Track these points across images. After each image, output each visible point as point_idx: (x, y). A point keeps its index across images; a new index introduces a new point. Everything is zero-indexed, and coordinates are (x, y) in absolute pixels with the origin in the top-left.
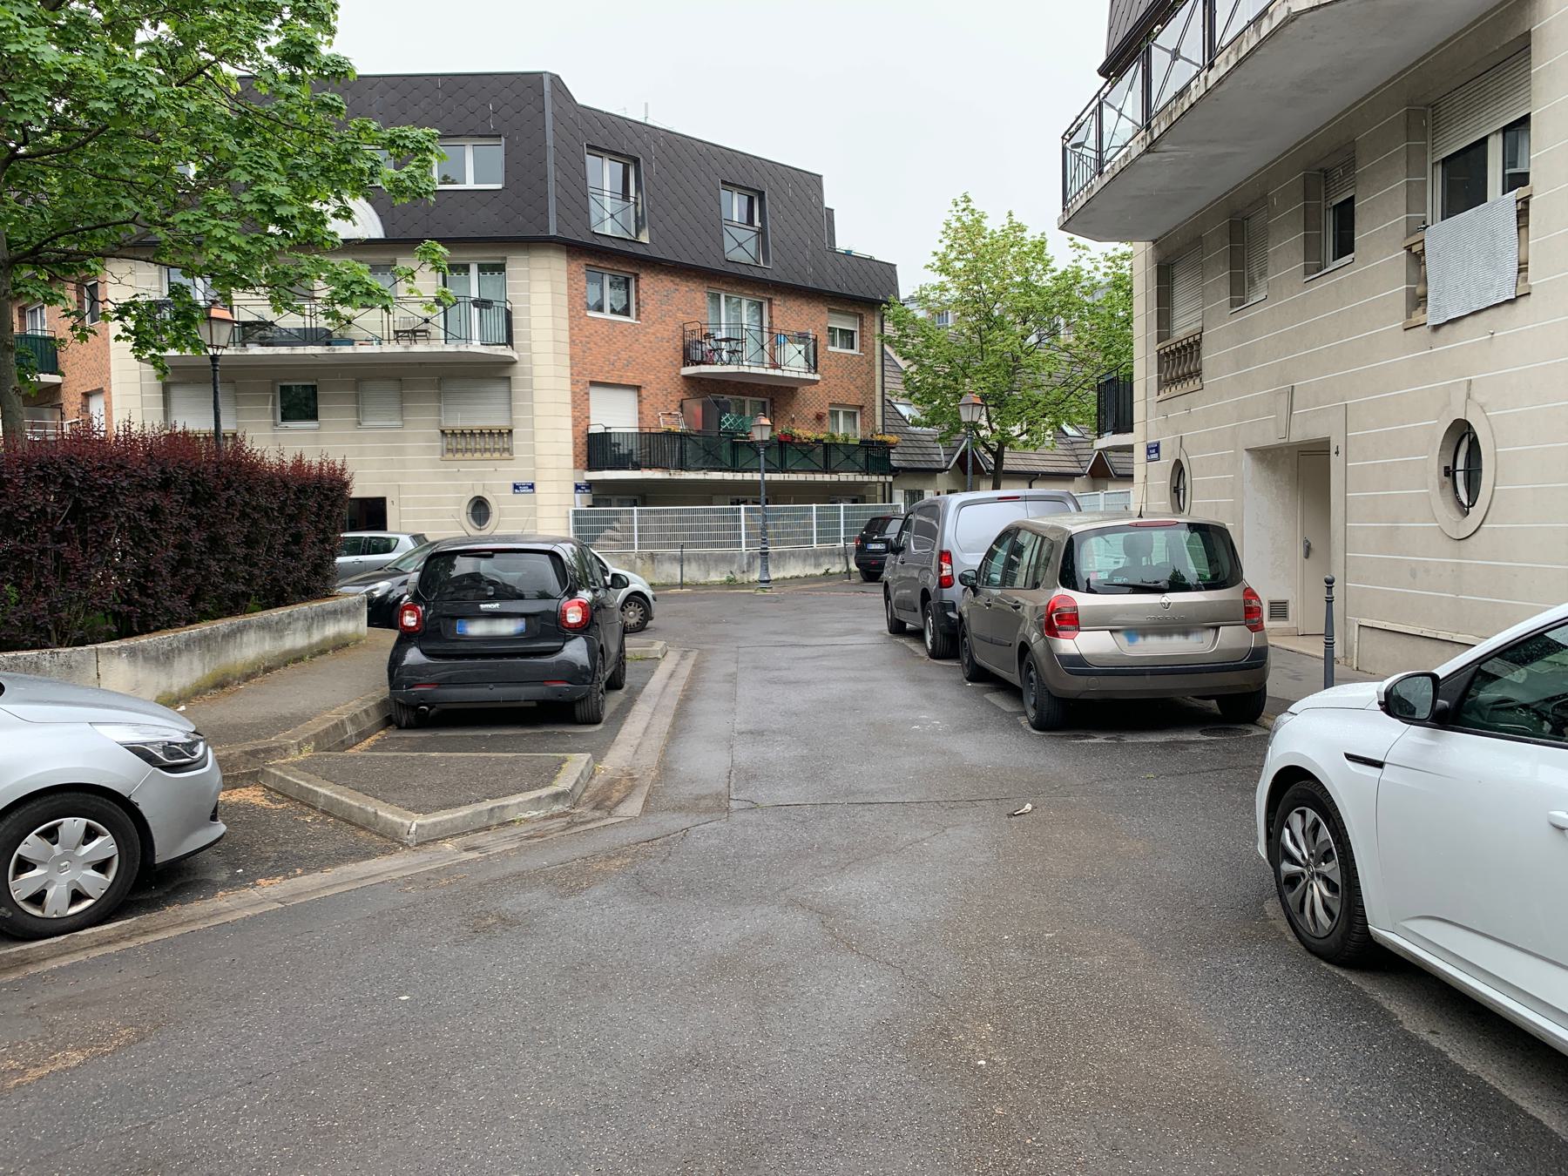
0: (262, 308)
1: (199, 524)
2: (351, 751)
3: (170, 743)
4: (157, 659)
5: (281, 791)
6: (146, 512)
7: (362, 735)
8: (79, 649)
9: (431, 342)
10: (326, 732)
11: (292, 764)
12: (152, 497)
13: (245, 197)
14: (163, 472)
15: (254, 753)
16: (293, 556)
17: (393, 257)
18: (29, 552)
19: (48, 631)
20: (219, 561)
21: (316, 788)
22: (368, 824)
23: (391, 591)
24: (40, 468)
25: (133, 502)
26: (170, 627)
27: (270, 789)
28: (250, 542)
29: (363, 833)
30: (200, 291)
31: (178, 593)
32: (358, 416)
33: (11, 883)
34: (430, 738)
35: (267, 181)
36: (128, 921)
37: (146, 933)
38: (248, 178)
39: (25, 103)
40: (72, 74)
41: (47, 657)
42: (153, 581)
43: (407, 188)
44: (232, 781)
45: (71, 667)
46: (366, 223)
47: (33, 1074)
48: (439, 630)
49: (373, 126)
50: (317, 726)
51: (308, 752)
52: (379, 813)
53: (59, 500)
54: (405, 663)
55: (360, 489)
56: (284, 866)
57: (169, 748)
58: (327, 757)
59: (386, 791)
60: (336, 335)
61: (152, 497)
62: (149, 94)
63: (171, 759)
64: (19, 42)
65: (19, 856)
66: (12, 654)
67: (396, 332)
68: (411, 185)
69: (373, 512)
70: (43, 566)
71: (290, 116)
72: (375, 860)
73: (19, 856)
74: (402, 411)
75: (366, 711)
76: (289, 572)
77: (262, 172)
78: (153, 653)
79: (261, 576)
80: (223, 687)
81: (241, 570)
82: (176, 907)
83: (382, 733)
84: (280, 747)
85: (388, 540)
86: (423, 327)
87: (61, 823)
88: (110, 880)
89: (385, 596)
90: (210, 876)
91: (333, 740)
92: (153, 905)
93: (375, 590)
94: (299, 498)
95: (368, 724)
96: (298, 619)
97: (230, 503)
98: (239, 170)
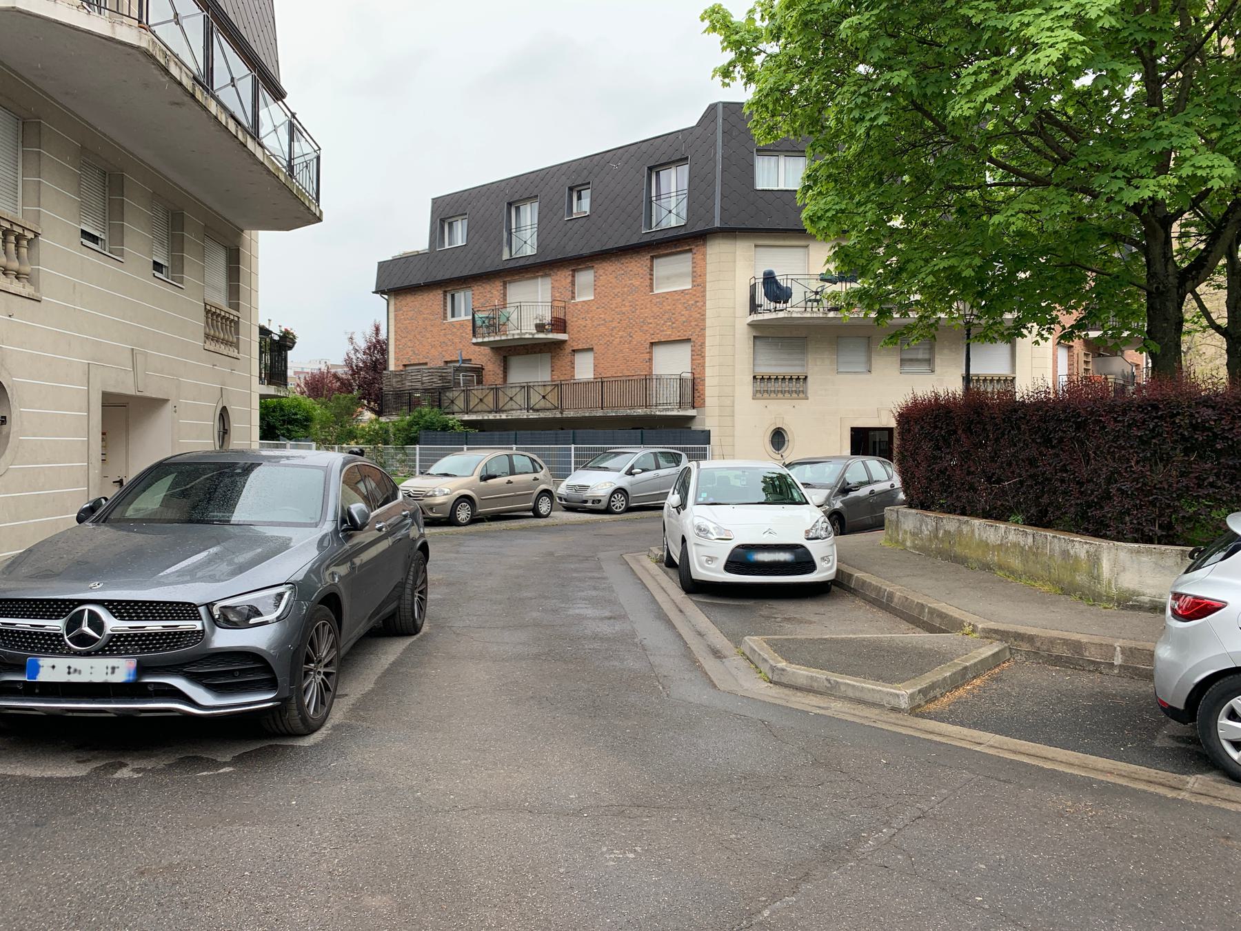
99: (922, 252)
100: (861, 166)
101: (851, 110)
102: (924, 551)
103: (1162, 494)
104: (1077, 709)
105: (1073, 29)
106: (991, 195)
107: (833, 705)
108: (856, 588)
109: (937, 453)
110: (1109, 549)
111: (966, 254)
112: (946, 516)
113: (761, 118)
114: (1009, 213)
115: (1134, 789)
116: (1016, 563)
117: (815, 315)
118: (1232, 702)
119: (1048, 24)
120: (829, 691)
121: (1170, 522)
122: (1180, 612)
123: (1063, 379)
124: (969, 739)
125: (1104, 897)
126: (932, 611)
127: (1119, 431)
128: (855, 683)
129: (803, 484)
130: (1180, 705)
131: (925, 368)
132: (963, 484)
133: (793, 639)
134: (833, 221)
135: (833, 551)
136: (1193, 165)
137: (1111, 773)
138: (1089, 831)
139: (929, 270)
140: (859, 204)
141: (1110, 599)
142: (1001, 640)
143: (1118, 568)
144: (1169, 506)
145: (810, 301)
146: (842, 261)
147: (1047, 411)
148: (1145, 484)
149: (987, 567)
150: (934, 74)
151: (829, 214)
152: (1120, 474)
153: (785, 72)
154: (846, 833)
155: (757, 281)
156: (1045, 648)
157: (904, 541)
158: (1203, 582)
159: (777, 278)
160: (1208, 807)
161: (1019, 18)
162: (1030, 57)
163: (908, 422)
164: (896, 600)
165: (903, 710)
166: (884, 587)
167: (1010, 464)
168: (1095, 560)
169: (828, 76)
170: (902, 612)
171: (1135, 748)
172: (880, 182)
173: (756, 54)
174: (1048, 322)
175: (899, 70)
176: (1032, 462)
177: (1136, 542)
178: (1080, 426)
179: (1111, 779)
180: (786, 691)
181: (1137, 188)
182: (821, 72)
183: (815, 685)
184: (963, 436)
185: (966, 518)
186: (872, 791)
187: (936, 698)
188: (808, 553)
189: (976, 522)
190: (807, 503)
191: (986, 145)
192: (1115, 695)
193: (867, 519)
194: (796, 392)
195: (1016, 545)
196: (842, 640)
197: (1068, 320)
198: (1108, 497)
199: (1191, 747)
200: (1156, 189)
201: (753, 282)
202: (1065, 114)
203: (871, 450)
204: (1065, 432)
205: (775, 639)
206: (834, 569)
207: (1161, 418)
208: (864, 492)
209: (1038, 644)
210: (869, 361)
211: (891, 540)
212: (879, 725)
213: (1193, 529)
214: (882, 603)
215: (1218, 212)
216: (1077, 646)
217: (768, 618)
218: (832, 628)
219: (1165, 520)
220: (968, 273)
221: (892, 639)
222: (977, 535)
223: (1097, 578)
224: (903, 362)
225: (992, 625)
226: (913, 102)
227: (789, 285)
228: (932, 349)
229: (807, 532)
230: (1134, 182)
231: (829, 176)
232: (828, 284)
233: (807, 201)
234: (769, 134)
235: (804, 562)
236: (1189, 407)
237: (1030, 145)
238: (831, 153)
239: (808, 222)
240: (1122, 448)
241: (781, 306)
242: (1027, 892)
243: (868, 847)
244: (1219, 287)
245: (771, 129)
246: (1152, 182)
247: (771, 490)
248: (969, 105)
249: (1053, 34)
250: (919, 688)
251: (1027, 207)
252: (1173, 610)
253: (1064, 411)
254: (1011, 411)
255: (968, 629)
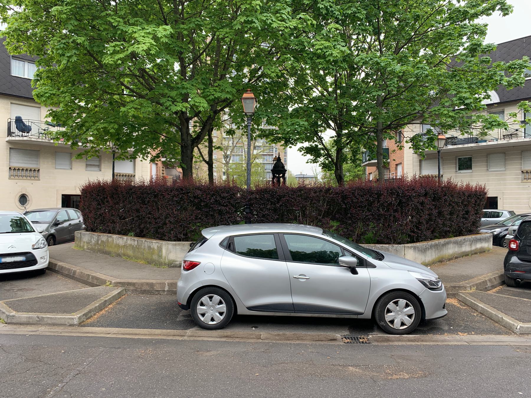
0: (453, 132)
1: (435, 207)
2: (488, 292)
3: (431, 281)
4: (422, 251)
5: (464, 302)
6: (420, 203)
7: (493, 287)
8: (399, 245)
9: (518, 138)
10: (480, 283)
11: (468, 293)
12: (422, 199)
13: (455, 99)
14: (425, 191)
15: (455, 287)
16: (466, 219)
17: (503, 108)
18: (387, 215)
19: (391, 239)
20: (441, 220)
21: (478, 304)
22: (499, 321)
23: (501, 233)
24: (391, 190)
25: (416, 200)
26: (425, 240)
27: (460, 301)
28: (451, 214)
29: (497, 324)
30: (435, 131)
31: (428, 229)
32: (487, 167)
33: (385, 315)
34: (522, 292)
35: (462, 92)
36: (417, 336)
37: (422, 341)
38: (455, 92)
39: (391, 84)
40: (404, 72)
41: (391, 247)
42: (421, 225)
43: (513, 83)
44: (449, 296)
45: (397, 251)
46: (495, 98)
47: (395, 377)
48: (526, 251)
49: (502, 63)
50: (476, 281)
51: (473, 290)
52: (504, 318)
53: (395, 200)
54: (511, 262)
55: (490, 194)
56: (467, 330)
57: (431, 282)
58: (481, 293)
59: (506, 310)
60: (480, 139)
61: (422, 199)
62: (426, 72)
63: (431, 286)
64: (391, 67)
65: (388, 308)
66: (381, 245)
67: (504, 136)
68: (514, 82)
69: (493, 202)
70: (390, 219)
71: (470, 68)
72: (503, 336)
73: (388, 308)
74: (505, 165)
75: (495, 278)
76: (464, 224)
77: (460, 90)
78: (420, 249)
79: (454, 225)
80: (441, 262)
81: (448, 223)
82: (432, 335)
83: (501, 287)
84: (464, 287)
85: (499, 213)
86: (515, 133)
87: (399, 300)
88: (412, 321)
89: (499, 234)
90: (442, 327)
91: (482, 287)
92: (424, 332)
93: (494, 232)
94: (468, 198)
95: (496, 283)
96: (467, 241)
97: (446, 201)
98: (453, 91)
99: (92, 119)
100: (64, 76)
101: (58, 49)
102: (93, 250)
103: (184, 223)
104: (150, 311)
105: (152, 39)
106: (124, 98)
107: (40, 329)
108: (59, 270)
109: (99, 207)
110: (165, 244)
111: (111, 122)
112: (102, 234)
113: (11, 41)
114: (128, 107)
115: (168, 340)
116: (130, 252)
117: (44, 141)
118: (201, 299)
119: (143, 34)
120: (39, 322)
121: (187, 233)
122: (186, 267)
123: (154, 177)
124: (105, 332)
125: (152, 388)
126: (93, 277)
127: (169, 198)
128: (52, 316)
129: (32, 222)
130: (185, 303)
131: (97, 169)
132: (110, 220)
133: (21, 300)
134: (49, 98)
135: (47, 254)
136: (194, 101)
137: (160, 335)
138: (149, 361)
139: (95, 127)
140: (63, 92)
141: (165, 264)
142: (122, 286)
143: (169, 252)
144: (186, 227)
145: (41, 133)
146: (54, 117)
147: (143, 190)
148: (178, 219)
149: (119, 255)
150: (98, 42)
151: (47, 95)
152: (169, 215)
153: (24, 22)
154: (39, 392)
155: (12, 120)
156: (139, 287)
157: (84, 246)
158: (193, 256)
159: (23, 120)
160: (194, 340)
161: (132, 29)
162: (136, 46)
163: (86, 193)
164: (77, 274)
165: (75, 325)
166: (72, 268)
167: (129, 212)
168: (160, 249)
169: (46, 30)
170: (80, 279)
171: (170, 323)
172: (73, 84)
173: (8, 9)
174: (145, 154)
175: (81, 36)
176: (138, 211)
177: (175, 241)
178: (155, 196)
179: (160, 337)
180: (15, 326)
181: (176, 106)
182: (42, 27)
183: (31, 320)
184: (110, 199)
185: (110, 235)
186: (55, 367)
187: (91, 316)
188: (33, 256)
189: (115, 236)
190: (34, 231)
191: (119, 78)
192: (165, 303)
193: (67, 237)
194: (21, 176)
195: (130, 245)
196: (48, 296)
197: (154, 153)
198: (165, 224)
199: (189, 318)
200: (182, 107)
201: (9, 120)
202: (154, 72)
203: (72, 205)
204: (150, 198)
205: (10, 301)
206: (48, 262)
207: (184, 194)
208: (66, 224)
209: (137, 286)
210: (71, 164)
211: (77, 246)
212: (63, 334)
213: (194, 235)
214: (71, 276)
215: (205, 119)
216: (152, 285)
217: (9, 290)
218: (44, 291)
219: (185, 232)
220: (112, 131)
221: (73, 292)
222: (115, 242)
223: (160, 256)
224: (87, 165)
225: (118, 280)
226: (88, 51)
227: (30, 125)
228: (100, 161)
229: (33, 245)
230: (175, 103)
231: (48, 77)
232: (51, 127)
233: (37, 86)
234: (15, 50)
235: (31, 260)
236: (193, 190)
237: (139, 81)
238: (48, 67)
239: (36, 96)
240: (171, 205)
241: (26, 134)
242: (122, 395)
243: (50, 396)
244: (206, 146)
245: (16, 48)
246: (181, 104)
247: (15, 226)
248: (111, 59)
249: (145, 39)
250: (83, 313)
251: (136, 106)
252: (184, 267)
253: (150, 190)
254: (129, 190)
255: (108, 283)
